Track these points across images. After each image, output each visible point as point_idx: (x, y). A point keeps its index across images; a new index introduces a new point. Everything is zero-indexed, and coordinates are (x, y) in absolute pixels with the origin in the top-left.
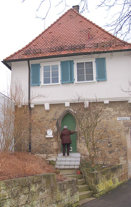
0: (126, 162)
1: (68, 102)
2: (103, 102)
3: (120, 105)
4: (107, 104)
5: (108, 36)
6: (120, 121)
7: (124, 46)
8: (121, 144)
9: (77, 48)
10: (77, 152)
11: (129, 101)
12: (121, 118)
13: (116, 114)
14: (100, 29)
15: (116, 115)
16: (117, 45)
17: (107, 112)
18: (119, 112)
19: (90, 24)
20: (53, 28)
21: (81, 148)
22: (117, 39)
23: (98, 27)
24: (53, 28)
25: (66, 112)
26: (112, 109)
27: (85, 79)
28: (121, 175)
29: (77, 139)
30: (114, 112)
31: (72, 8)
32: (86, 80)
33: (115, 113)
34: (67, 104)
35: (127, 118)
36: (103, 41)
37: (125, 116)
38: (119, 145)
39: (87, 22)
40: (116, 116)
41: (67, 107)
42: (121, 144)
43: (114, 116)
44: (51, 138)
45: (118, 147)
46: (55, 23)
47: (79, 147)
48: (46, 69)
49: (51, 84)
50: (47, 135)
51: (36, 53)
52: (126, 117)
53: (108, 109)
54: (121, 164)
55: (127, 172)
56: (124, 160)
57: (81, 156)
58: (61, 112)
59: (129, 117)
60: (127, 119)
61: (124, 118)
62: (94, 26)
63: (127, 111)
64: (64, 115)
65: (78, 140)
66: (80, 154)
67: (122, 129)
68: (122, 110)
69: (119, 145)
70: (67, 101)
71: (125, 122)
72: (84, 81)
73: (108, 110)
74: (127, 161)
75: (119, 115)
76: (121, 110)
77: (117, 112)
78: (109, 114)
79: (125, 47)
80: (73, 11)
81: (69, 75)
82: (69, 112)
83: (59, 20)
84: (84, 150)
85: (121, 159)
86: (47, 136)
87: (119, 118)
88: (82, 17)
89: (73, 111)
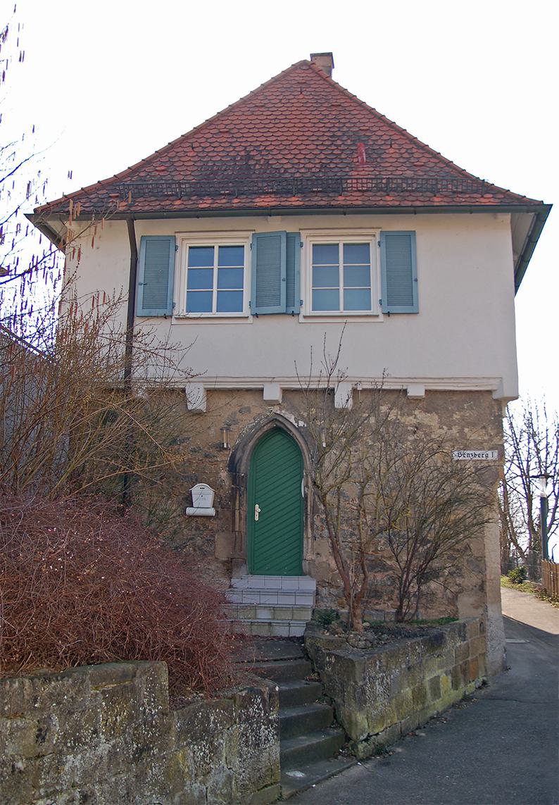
2: (405, 391)
4: (417, 400)
7: (482, 197)
8: (466, 548)
10: (305, 575)
18: (461, 432)
29: (307, 525)
34: (273, 393)
35: (490, 453)
36: (409, 173)
41: (272, 403)
47: (314, 557)
48: (200, 254)
58: (249, 421)
61: (477, 453)
65: (310, 530)
70: (272, 380)
74: (486, 610)
76: (468, 424)
82: (279, 424)
86: (190, 511)
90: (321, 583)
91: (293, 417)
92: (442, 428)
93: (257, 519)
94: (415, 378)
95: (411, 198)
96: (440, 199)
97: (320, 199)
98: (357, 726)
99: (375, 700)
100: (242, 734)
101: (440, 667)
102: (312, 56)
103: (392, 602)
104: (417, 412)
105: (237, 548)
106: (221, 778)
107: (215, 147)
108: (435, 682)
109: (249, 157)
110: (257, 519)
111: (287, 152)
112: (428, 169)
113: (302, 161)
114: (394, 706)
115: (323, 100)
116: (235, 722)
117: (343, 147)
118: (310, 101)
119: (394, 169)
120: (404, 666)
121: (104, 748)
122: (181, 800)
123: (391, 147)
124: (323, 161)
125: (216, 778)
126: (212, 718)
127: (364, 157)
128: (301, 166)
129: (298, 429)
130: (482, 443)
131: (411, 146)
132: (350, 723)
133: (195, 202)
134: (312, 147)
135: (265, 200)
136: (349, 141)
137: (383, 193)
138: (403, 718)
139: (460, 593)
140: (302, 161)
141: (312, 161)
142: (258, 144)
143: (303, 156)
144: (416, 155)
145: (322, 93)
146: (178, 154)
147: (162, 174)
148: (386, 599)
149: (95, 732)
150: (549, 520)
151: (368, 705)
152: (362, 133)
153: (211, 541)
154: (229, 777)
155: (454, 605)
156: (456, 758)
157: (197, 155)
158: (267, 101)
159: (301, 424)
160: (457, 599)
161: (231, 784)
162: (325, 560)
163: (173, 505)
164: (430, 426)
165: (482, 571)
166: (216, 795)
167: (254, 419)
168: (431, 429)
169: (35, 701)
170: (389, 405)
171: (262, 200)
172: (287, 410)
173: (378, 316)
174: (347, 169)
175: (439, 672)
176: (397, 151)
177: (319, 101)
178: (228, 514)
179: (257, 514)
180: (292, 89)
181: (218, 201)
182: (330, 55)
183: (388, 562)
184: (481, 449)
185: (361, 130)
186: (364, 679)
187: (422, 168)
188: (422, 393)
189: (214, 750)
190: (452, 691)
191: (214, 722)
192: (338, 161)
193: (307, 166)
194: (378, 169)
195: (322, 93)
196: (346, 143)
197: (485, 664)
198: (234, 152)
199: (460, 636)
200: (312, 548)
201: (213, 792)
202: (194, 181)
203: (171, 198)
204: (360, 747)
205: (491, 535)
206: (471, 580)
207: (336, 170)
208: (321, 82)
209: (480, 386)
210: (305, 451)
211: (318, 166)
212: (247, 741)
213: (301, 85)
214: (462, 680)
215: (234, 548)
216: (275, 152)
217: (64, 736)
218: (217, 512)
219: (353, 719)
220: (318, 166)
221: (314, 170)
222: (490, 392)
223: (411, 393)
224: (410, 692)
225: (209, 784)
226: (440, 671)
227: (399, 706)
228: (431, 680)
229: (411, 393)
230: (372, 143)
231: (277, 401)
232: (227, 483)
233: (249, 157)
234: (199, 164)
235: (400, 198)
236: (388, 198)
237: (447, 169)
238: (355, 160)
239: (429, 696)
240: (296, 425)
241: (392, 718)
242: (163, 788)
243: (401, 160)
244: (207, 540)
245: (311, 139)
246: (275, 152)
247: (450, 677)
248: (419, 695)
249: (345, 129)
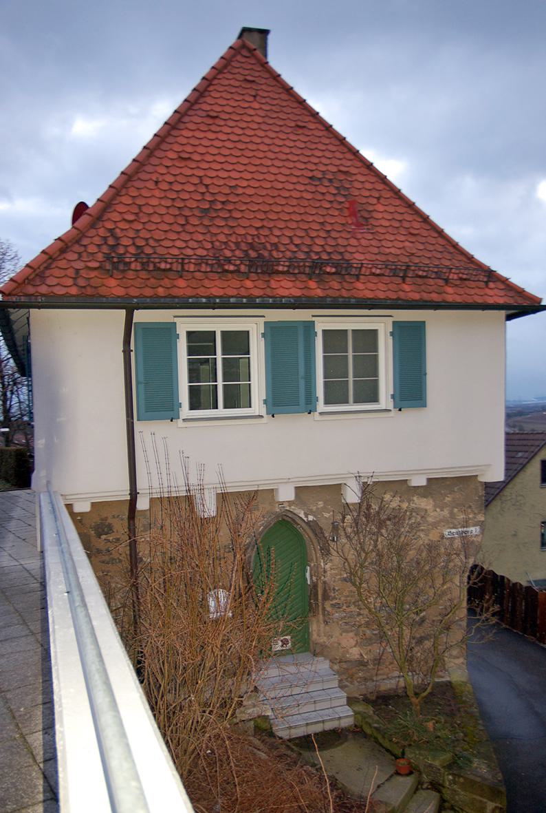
2: (264, 400)
3: (456, 489)
14: (277, 81)
15: (442, 521)
18: (451, 513)
23: (266, 68)
27: (351, 398)
30: (435, 513)
32: (356, 402)
34: (286, 494)
43: (435, 525)
48: (200, 343)
49: (221, 411)
58: (258, 521)
59: (477, 525)
66: (328, 661)
72: (346, 402)
77: (446, 512)
81: (302, 383)
84: (339, 644)
87: (449, 530)
89: (302, 515)
91: (303, 512)
92: (436, 511)
104: (415, 498)
129: (308, 523)
156: (322, 791)
159: (311, 518)
170: (392, 494)
185: (340, 171)
188: (424, 483)
237: (440, 241)
240: (305, 519)
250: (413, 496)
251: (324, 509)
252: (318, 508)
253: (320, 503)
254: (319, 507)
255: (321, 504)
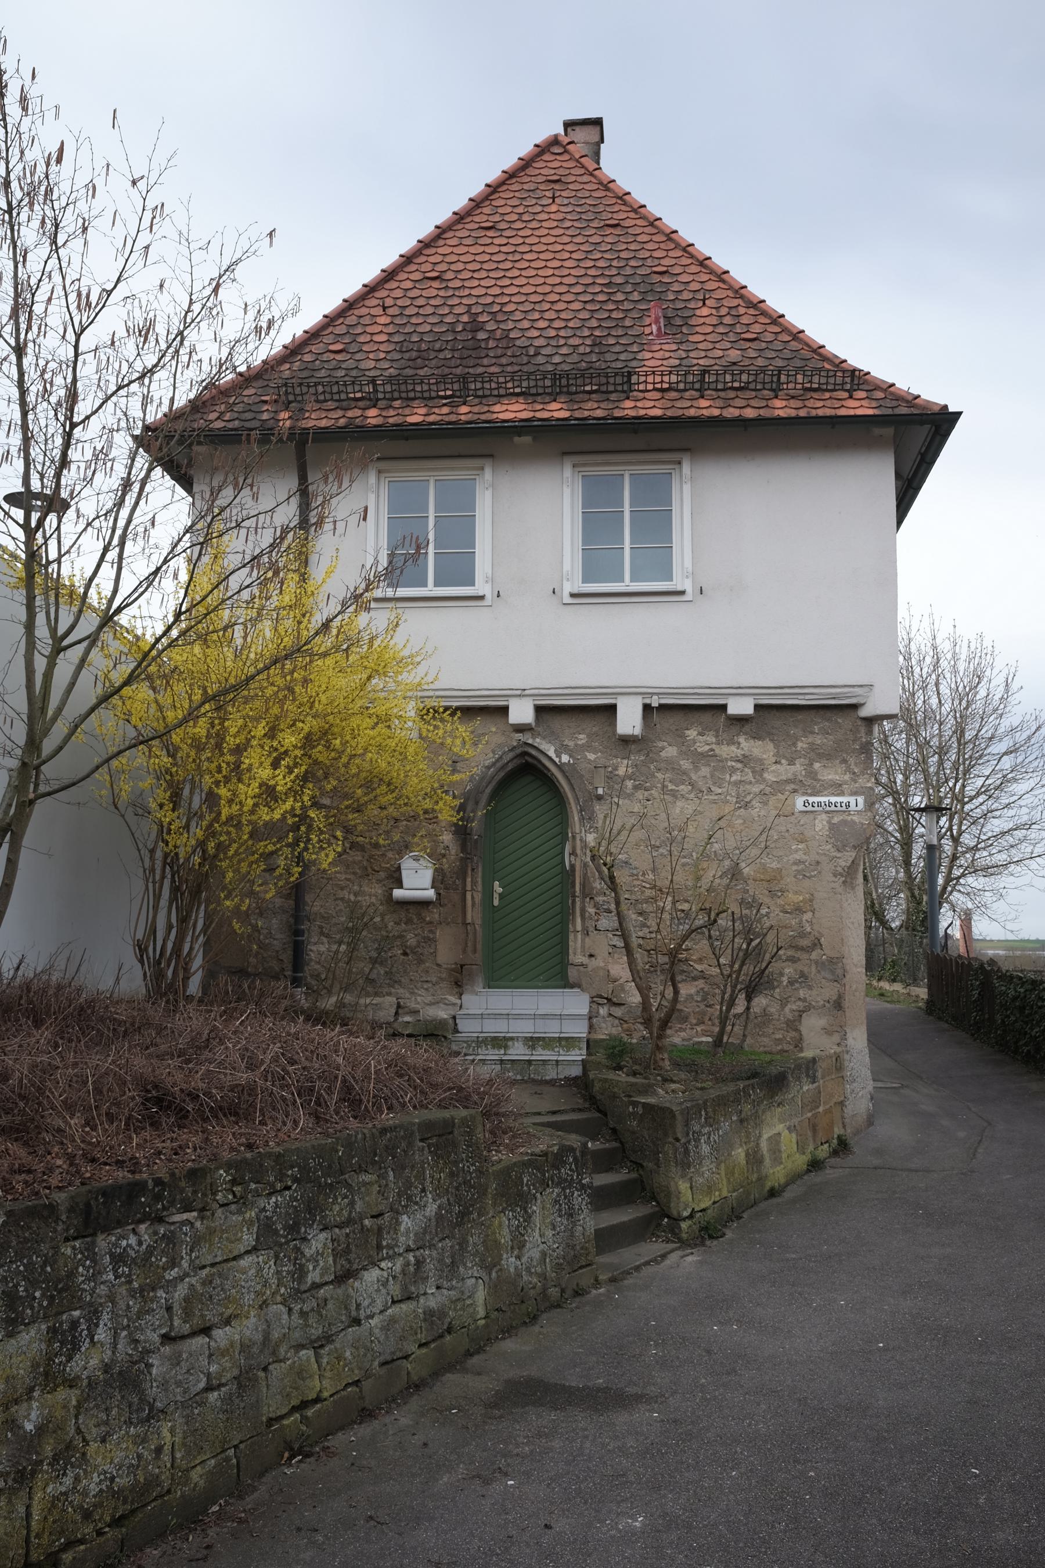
0: (839, 1044)
1: (524, 699)
2: (723, 707)
4: (741, 720)
5: (624, 215)
6: (812, 816)
7: (851, 397)
8: (815, 945)
9: (588, 388)
10: (572, 987)
11: (863, 705)
12: (816, 799)
13: (790, 776)
15: (788, 781)
16: (816, 386)
17: (739, 765)
19: (662, 246)
20: (448, 250)
21: (593, 963)
22: (635, 211)
24: (448, 250)
25: (511, 755)
26: (770, 746)
28: (809, 1115)
29: (574, 912)
31: (562, 133)
33: (784, 771)
34: (522, 713)
35: (852, 800)
36: (734, 355)
37: (837, 788)
38: (802, 949)
39: (647, 230)
40: (793, 786)
41: (520, 729)
42: (815, 945)
43: (778, 786)
44: (423, 904)
45: (799, 959)
46: (462, 218)
47: (585, 960)
50: (401, 886)
51: (349, 399)
52: (842, 794)
53: (746, 745)
54: (808, 1054)
55: (842, 1098)
56: (828, 1032)
57: (594, 1006)
60: (848, 805)
61: (833, 799)
62: (689, 261)
63: (852, 761)
64: (502, 774)
65: (579, 921)
67: (818, 863)
68: (826, 756)
69: (802, 949)
70: (522, 694)
71: (835, 820)
73: (747, 753)
74: (844, 1037)
75: (812, 785)
76: (821, 756)
77: (798, 768)
78: (750, 777)
79: (856, 404)
80: (566, 151)
82: (530, 760)
83: (482, 201)
85: (813, 1025)
86: (398, 893)
87: (805, 798)
88: (635, 211)
89: (552, 753)
90: (596, 1000)
91: (552, 749)
93: (496, 903)
94: (740, 688)
95: (739, 403)
96: (784, 403)
97: (596, 405)
98: (679, 1199)
99: (700, 1164)
100: (556, 1201)
101: (782, 1120)
102: (569, 125)
103: (703, 1027)
105: (469, 949)
106: (536, 1254)
107: (420, 307)
108: (775, 1139)
109: (475, 326)
110: (496, 903)
111: (537, 316)
112: (764, 345)
113: (562, 333)
114: (723, 1173)
115: (590, 214)
116: (548, 1186)
117: (627, 306)
118: (569, 217)
119: (711, 346)
120: (734, 1118)
121: (432, 1209)
122: (498, 1277)
123: (704, 304)
124: (597, 333)
125: (533, 1253)
126: (525, 1180)
127: (662, 325)
128: (562, 342)
129: (560, 767)
130: (840, 785)
131: (736, 302)
132: (669, 1195)
133: (400, 411)
134: (576, 306)
135: (510, 407)
136: (636, 293)
137: (694, 392)
138: (734, 1191)
139: (804, 1012)
140: (562, 333)
141: (578, 333)
142: (489, 300)
143: (563, 324)
144: (745, 320)
145: (588, 201)
146: (362, 321)
147: (339, 357)
148: (694, 1021)
149: (423, 1190)
150: (940, 881)
151: (692, 1170)
152: (656, 278)
153: (430, 941)
154: (544, 1254)
155: (797, 1030)
157: (392, 322)
158: (497, 218)
159: (565, 758)
160: (800, 1021)
161: (545, 1262)
162: (602, 964)
163: (373, 891)
164: (761, 760)
165: (838, 979)
166: (530, 1274)
167: (493, 752)
168: (763, 764)
169: (375, 1155)
171: (505, 407)
172: (544, 738)
173: (682, 593)
174: (635, 348)
175: (780, 1128)
176: (714, 312)
177: (583, 217)
178: (456, 897)
179: (496, 896)
180: (539, 194)
181: (436, 410)
182: (598, 122)
183: (697, 966)
184: (838, 795)
186: (688, 1134)
187: (755, 345)
189: (528, 1219)
190: (797, 1155)
191: (527, 1185)
192: (620, 332)
193: (571, 341)
194: (684, 347)
195: (588, 201)
196: (631, 298)
197: (843, 1117)
198: (451, 316)
199: (808, 1076)
200: (583, 947)
201: (528, 1270)
202: (392, 370)
203: (361, 404)
204: (684, 1225)
205: (853, 923)
206: (823, 992)
207: (617, 349)
208: (586, 178)
209: (838, 698)
210: (572, 801)
211: (588, 342)
212: (560, 1210)
213: (553, 185)
214: (811, 1139)
215: (464, 951)
216: (518, 316)
217: (398, 1193)
218: (438, 894)
219: (673, 1189)
220: (588, 342)
221: (581, 350)
222: (855, 707)
223: (732, 710)
224: (743, 1155)
225: (524, 1260)
226: (782, 1126)
227: (730, 1173)
228: (770, 1138)
229: (732, 710)
230: (672, 298)
231: (530, 724)
232: (454, 850)
233: (475, 326)
234: (396, 340)
235: (719, 403)
236: (703, 403)
237: (794, 345)
238: (647, 330)
239: (767, 1161)
240: (557, 760)
241: (720, 1190)
242: (482, 1260)
243: (721, 329)
244: (424, 938)
245: (574, 290)
246: (518, 316)
247: (794, 1135)
248: (754, 1159)
249: (628, 271)
250: (738, 735)
251: (588, 747)
252: (576, 745)
253: (581, 736)
254: (580, 742)
255: (582, 739)
